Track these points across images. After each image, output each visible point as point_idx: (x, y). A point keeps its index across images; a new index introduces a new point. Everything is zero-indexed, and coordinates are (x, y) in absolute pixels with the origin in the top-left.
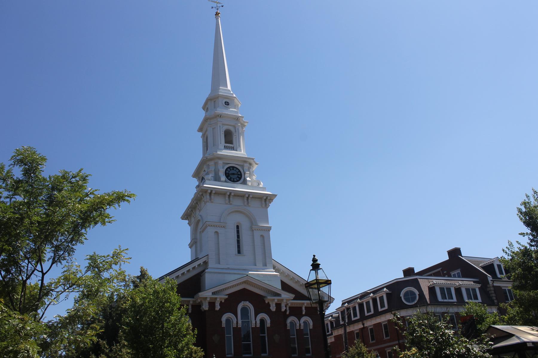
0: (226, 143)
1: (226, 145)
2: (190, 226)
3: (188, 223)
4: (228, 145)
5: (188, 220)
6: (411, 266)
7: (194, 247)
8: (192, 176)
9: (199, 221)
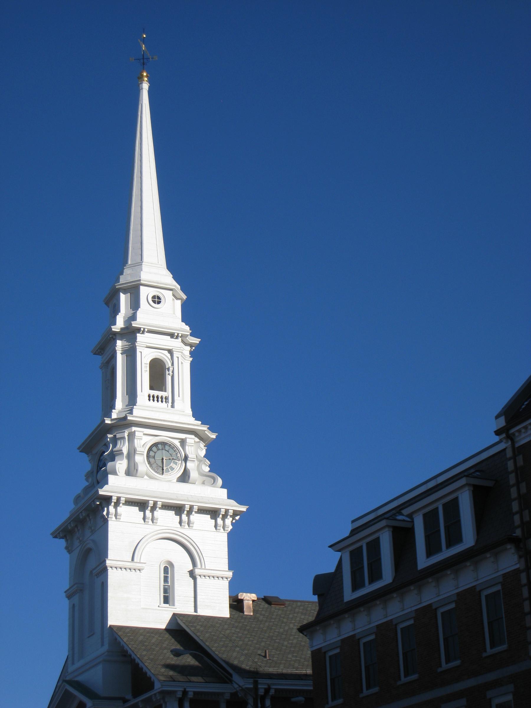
0: (151, 388)
1: (153, 392)
2: (69, 554)
3: (66, 548)
4: (156, 393)
5: (67, 541)
6: (314, 596)
7: (76, 599)
8: (79, 449)
9: (89, 551)
